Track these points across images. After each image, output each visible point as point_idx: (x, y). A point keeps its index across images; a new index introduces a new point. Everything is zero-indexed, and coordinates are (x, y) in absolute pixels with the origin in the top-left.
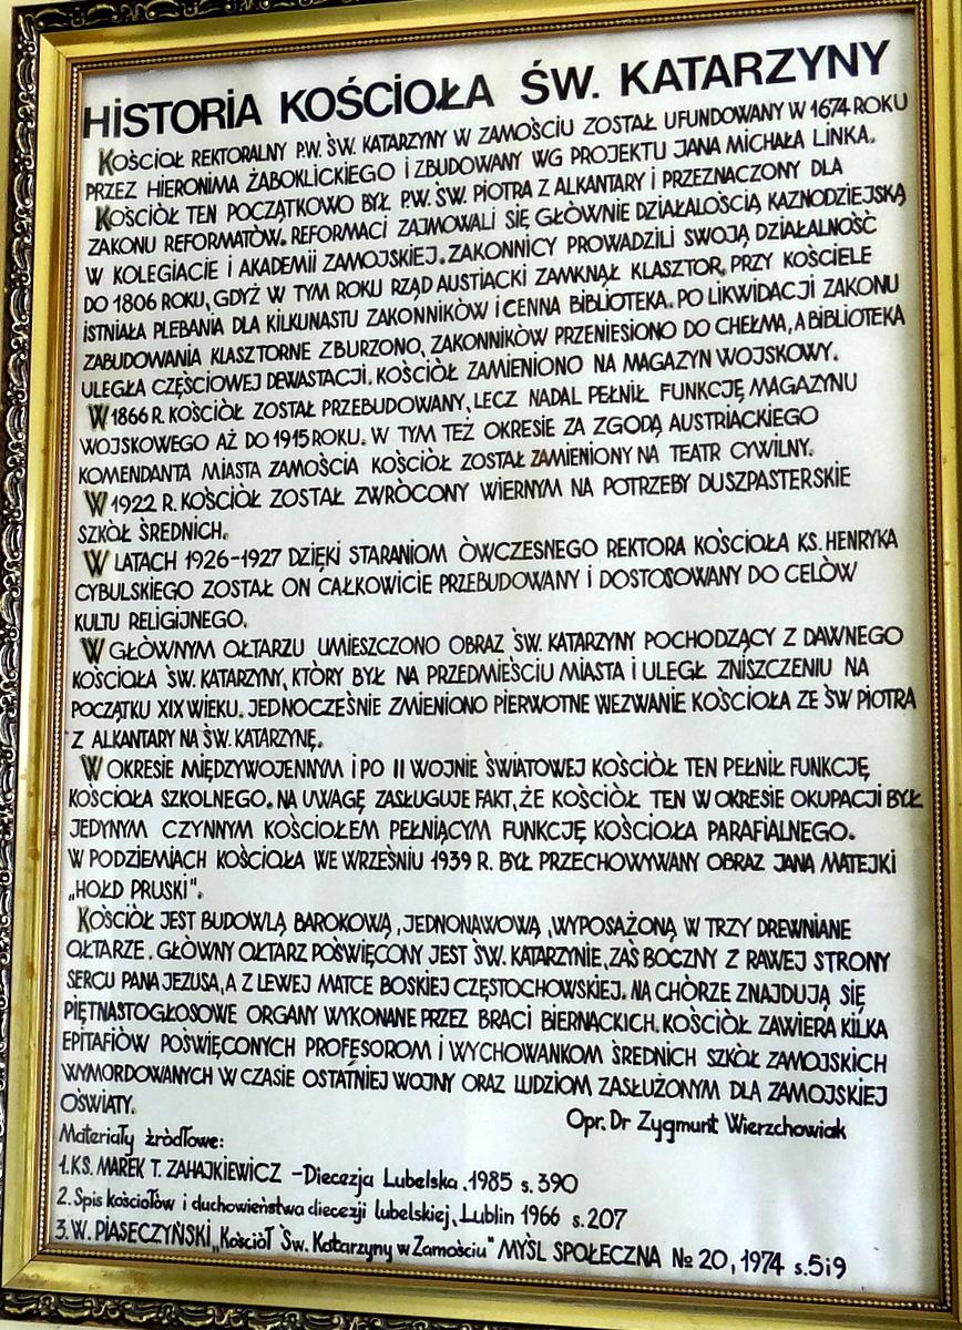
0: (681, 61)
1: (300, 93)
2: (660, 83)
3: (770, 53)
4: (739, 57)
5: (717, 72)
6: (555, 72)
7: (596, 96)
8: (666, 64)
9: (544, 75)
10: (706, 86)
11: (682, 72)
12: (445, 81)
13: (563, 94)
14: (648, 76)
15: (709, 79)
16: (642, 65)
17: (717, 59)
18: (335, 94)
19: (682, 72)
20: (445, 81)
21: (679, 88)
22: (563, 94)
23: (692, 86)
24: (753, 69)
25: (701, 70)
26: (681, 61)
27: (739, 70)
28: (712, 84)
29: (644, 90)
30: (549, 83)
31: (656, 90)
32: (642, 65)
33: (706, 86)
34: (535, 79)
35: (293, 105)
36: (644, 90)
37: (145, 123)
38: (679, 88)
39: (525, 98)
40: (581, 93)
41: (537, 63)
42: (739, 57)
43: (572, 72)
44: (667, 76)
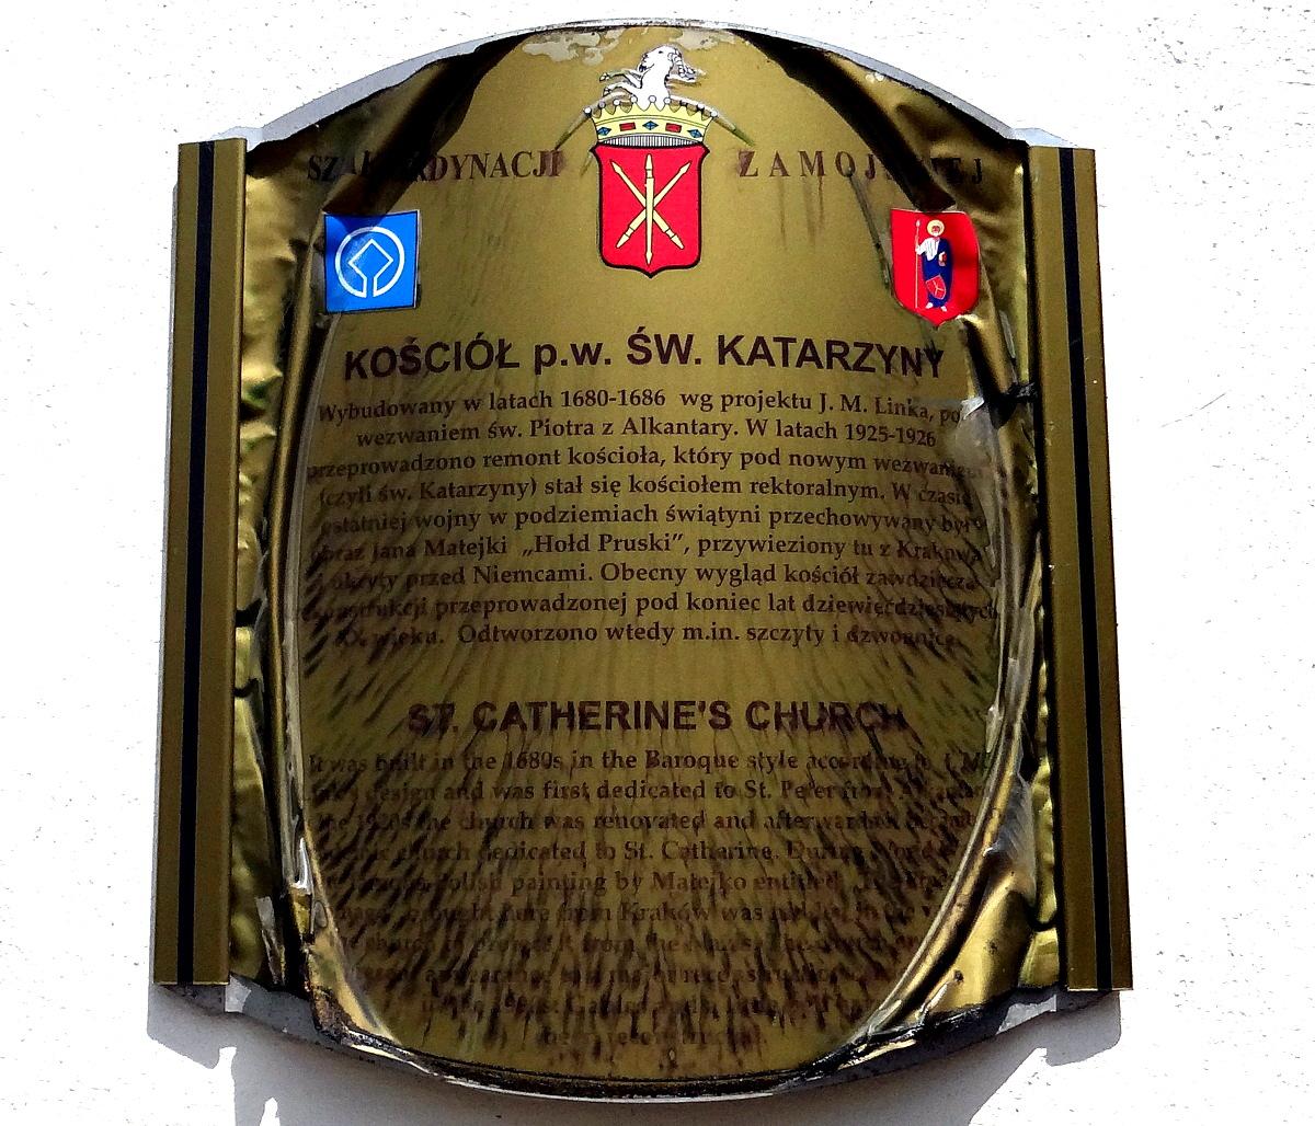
0: (776, 340)
1: (364, 353)
2: (754, 356)
3: (856, 344)
4: (830, 344)
5: (809, 353)
6: (658, 337)
7: (608, 362)
8: (760, 341)
9: (647, 340)
10: (799, 364)
11: (776, 350)
12: (501, 342)
13: (665, 358)
14: (745, 349)
15: (802, 358)
16: (738, 338)
17: (809, 343)
18: (397, 352)
19: (776, 350)
20: (501, 342)
21: (772, 363)
22: (665, 358)
23: (785, 364)
24: (841, 357)
25: (795, 351)
26: (776, 340)
27: (830, 355)
28: (756, 360)
29: (739, 361)
30: (652, 346)
31: (751, 362)
32: (738, 338)
33: (799, 364)
34: (639, 342)
35: (357, 363)
36: (739, 361)
37: (640, 543)
38: (772, 363)
39: (631, 357)
40: (684, 358)
41: (641, 329)
42: (830, 344)
43: (586, 347)
44: (761, 351)
